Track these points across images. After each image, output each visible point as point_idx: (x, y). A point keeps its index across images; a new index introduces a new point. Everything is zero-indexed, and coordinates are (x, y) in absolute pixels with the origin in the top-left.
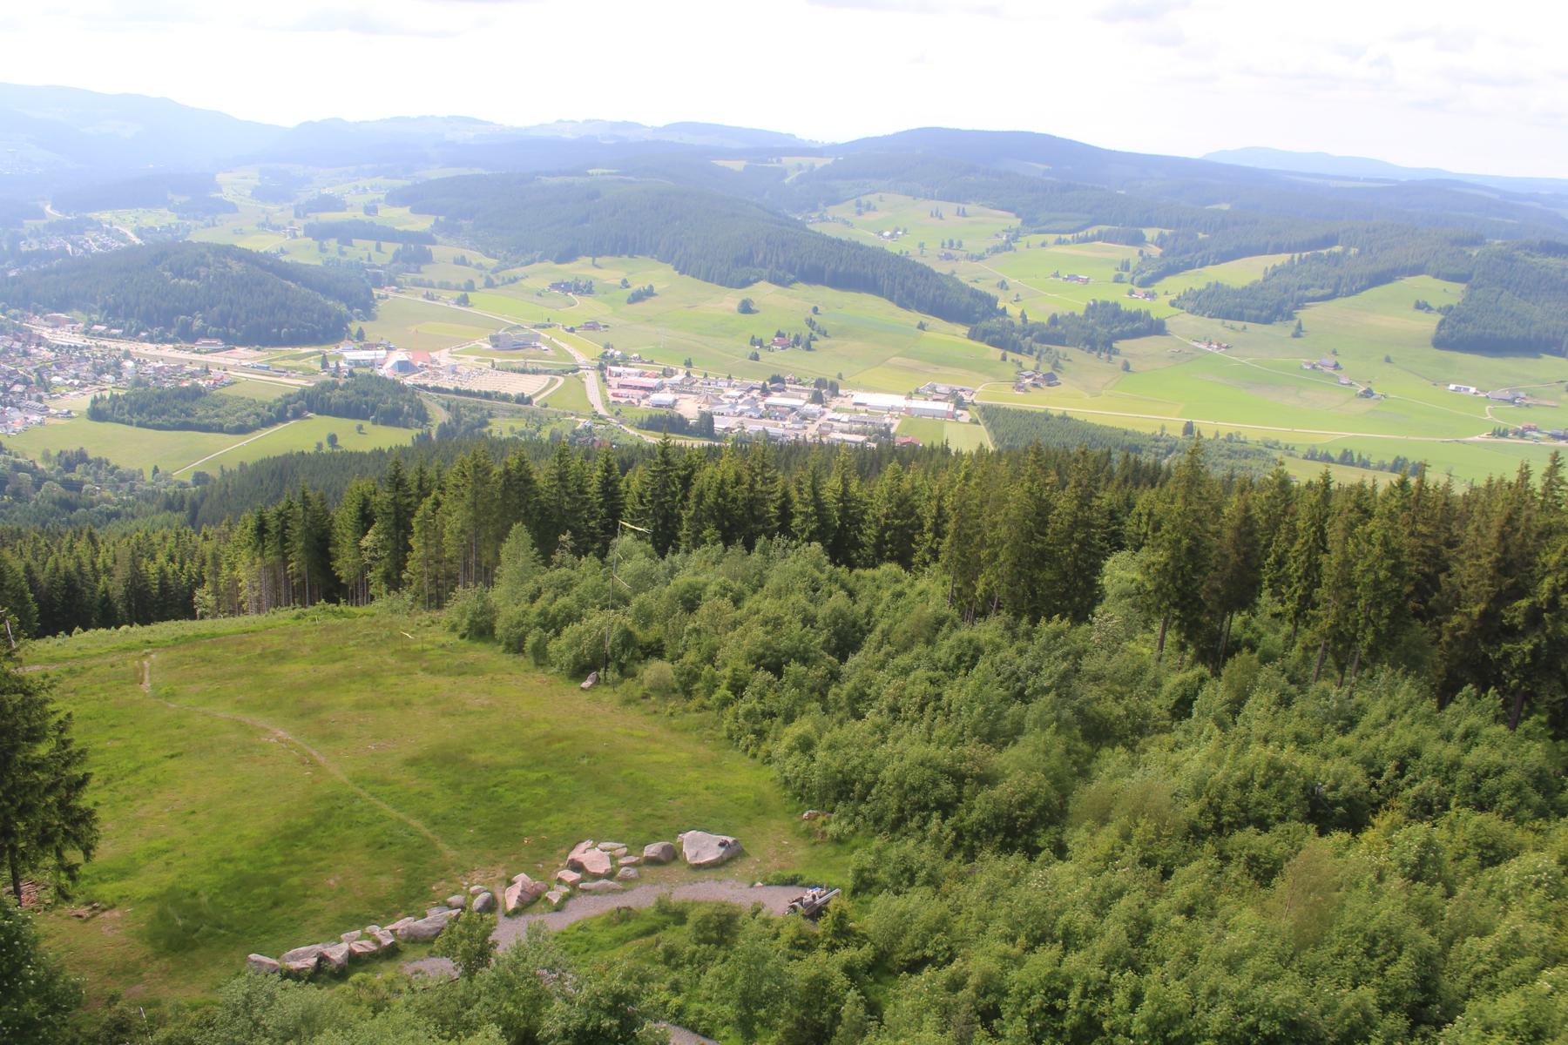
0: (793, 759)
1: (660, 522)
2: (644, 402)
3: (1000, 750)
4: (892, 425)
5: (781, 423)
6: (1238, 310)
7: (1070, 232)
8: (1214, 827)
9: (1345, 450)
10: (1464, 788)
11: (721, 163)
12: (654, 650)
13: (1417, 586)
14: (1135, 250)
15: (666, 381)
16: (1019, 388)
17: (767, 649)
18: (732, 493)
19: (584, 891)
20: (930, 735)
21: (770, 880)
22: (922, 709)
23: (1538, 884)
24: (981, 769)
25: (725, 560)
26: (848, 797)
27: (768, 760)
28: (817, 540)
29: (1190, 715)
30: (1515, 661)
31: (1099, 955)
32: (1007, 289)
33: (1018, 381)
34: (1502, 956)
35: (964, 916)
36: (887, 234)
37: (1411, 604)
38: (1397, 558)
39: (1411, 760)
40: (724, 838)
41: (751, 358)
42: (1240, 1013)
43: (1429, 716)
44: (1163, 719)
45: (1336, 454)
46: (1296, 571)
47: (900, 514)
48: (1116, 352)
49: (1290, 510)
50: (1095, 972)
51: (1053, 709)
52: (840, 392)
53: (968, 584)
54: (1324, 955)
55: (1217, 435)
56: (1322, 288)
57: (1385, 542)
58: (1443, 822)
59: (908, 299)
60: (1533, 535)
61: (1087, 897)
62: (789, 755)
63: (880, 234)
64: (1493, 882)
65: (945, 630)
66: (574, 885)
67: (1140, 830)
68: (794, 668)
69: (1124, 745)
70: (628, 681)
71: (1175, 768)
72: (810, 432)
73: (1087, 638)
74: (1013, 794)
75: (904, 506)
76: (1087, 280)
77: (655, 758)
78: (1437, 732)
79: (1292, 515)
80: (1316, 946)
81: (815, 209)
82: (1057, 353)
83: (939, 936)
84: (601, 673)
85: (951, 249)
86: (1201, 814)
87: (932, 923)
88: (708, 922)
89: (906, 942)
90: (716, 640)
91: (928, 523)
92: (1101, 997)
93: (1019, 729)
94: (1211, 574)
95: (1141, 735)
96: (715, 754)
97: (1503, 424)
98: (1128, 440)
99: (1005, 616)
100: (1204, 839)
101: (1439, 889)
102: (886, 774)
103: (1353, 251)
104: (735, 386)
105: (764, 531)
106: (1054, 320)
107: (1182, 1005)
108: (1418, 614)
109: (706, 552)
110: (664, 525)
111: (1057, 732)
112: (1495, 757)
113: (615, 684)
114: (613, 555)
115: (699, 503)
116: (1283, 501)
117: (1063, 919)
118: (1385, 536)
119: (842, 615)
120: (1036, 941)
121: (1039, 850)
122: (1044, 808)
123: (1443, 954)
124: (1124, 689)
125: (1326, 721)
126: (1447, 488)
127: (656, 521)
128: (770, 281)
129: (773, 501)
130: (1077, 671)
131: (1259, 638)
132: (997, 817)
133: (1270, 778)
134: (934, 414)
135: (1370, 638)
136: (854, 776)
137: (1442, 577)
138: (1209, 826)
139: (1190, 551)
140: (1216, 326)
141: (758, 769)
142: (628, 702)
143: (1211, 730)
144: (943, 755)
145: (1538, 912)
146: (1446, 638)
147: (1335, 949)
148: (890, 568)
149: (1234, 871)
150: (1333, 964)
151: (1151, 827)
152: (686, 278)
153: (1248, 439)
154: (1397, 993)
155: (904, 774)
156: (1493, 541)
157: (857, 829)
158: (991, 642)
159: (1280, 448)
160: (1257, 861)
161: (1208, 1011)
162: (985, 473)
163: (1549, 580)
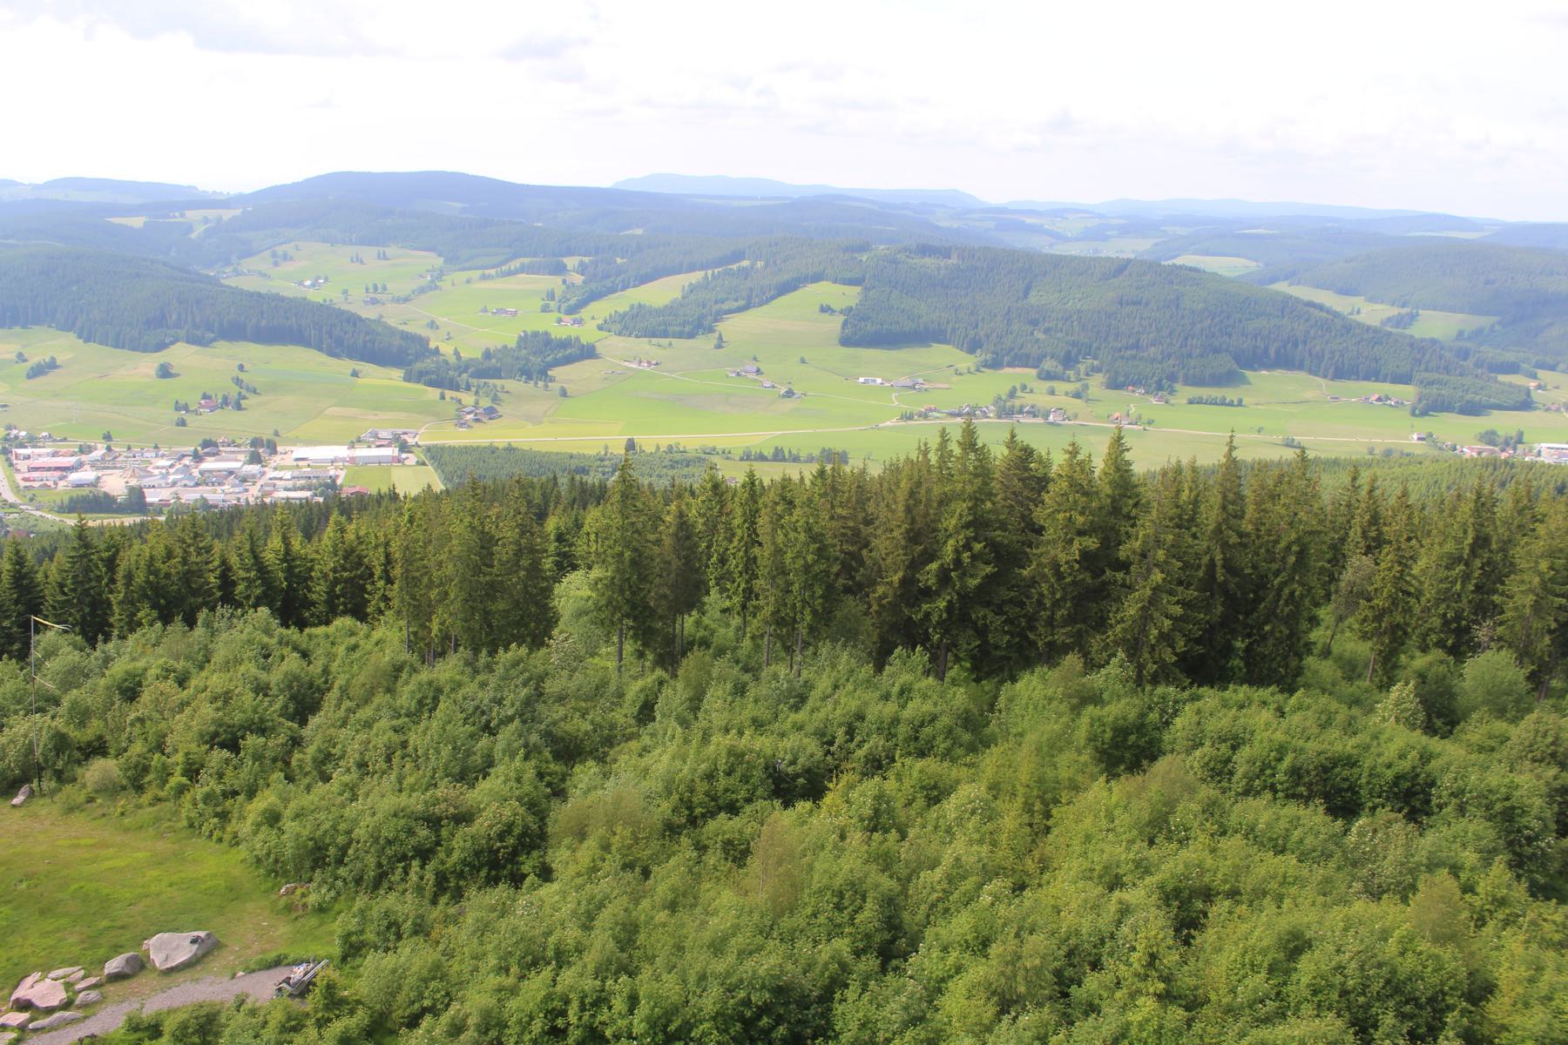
0: (261, 836)
1: (87, 610)
2: (62, 484)
3: (472, 786)
4: (337, 476)
5: (219, 489)
7: (493, 267)
8: (688, 821)
11: (117, 220)
12: (97, 749)
13: (843, 563)
14: (558, 280)
15: (84, 458)
16: (462, 425)
17: (221, 726)
18: (164, 568)
19: (35, 1030)
20: (400, 783)
21: (252, 966)
22: (389, 759)
23: (973, 812)
24: (456, 808)
25: (164, 640)
26: (325, 864)
27: (236, 841)
28: (266, 605)
29: (654, 719)
30: (935, 618)
31: (591, 967)
32: (438, 328)
33: (459, 418)
34: (950, 882)
35: (458, 958)
36: (308, 283)
37: (841, 581)
38: (821, 541)
40: (196, 934)
41: (178, 425)
42: (730, 990)
45: (768, 452)
46: (737, 566)
47: (348, 566)
48: (552, 380)
49: (725, 511)
50: (590, 984)
51: (520, 736)
52: (279, 449)
53: (423, 626)
54: (799, 920)
55: (658, 448)
56: (736, 300)
57: (809, 530)
58: (891, 774)
59: (337, 348)
60: (935, 505)
61: (574, 913)
62: (256, 833)
63: (301, 283)
64: (938, 818)
65: (404, 675)
66: (22, 1028)
67: (617, 837)
68: (252, 741)
69: (594, 758)
70: (68, 787)
71: (646, 772)
72: (252, 494)
73: (546, 661)
74: (491, 826)
75: (351, 557)
76: (515, 314)
77: (107, 864)
79: (727, 514)
80: (791, 912)
81: (228, 263)
82: (495, 386)
83: (433, 984)
84: (35, 784)
85: (375, 295)
86: (673, 811)
87: (425, 973)
88: (186, 1028)
89: (401, 998)
90: (163, 725)
91: (378, 571)
92: (599, 1007)
93: (489, 763)
94: (657, 581)
95: (611, 746)
96: (176, 847)
97: (908, 408)
98: (574, 463)
99: (464, 653)
100: (680, 834)
101: (893, 835)
102: (360, 833)
103: (760, 264)
104: (163, 456)
105: (205, 604)
106: (488, 355)
107: (676, 997)
108: (848, 590)
109: (144, 635)
110: (93, 614)
111: (526, 758)
112: (928, 707)
113: (53, 793)
114: (36, 654)
115: (128, 585)
116: (717, 503)
117: (552, 939)
119: (296, 678)
120: (534, 963)
121: (524, 876)
122: (524, 834)
123: (904, 892)
124: (589, 704)
125: (779, 702)
126: (863, 472)
127: (82, 609)
128: (188, 342)
129: (212, 571)
130: (542, 694)
131: (712, 635)
132: (477, 854)
134: (379, 461)
135: (808, 618)
136: (327, 841)
137: (864, 552)
138: (684, 821)
139: (634, 562)
140: (644, 346)
141: (227, 853)
142: (71, 810)
143: (674, 729)
144: (415, 802)
145: (976, 836)
146: (875, 607)
147: (809, 911)
148: (343, 622)
149: (711, 859)
150: (809, 924)
151: (627, 832)
152: (94, 346)
154: (868, 936)
155: (378, 829)
156: (900, 514)
157: (338, 894)
158: (452, 680)
161: (700, 996)
162: (424, 514)
163: (951, 542)
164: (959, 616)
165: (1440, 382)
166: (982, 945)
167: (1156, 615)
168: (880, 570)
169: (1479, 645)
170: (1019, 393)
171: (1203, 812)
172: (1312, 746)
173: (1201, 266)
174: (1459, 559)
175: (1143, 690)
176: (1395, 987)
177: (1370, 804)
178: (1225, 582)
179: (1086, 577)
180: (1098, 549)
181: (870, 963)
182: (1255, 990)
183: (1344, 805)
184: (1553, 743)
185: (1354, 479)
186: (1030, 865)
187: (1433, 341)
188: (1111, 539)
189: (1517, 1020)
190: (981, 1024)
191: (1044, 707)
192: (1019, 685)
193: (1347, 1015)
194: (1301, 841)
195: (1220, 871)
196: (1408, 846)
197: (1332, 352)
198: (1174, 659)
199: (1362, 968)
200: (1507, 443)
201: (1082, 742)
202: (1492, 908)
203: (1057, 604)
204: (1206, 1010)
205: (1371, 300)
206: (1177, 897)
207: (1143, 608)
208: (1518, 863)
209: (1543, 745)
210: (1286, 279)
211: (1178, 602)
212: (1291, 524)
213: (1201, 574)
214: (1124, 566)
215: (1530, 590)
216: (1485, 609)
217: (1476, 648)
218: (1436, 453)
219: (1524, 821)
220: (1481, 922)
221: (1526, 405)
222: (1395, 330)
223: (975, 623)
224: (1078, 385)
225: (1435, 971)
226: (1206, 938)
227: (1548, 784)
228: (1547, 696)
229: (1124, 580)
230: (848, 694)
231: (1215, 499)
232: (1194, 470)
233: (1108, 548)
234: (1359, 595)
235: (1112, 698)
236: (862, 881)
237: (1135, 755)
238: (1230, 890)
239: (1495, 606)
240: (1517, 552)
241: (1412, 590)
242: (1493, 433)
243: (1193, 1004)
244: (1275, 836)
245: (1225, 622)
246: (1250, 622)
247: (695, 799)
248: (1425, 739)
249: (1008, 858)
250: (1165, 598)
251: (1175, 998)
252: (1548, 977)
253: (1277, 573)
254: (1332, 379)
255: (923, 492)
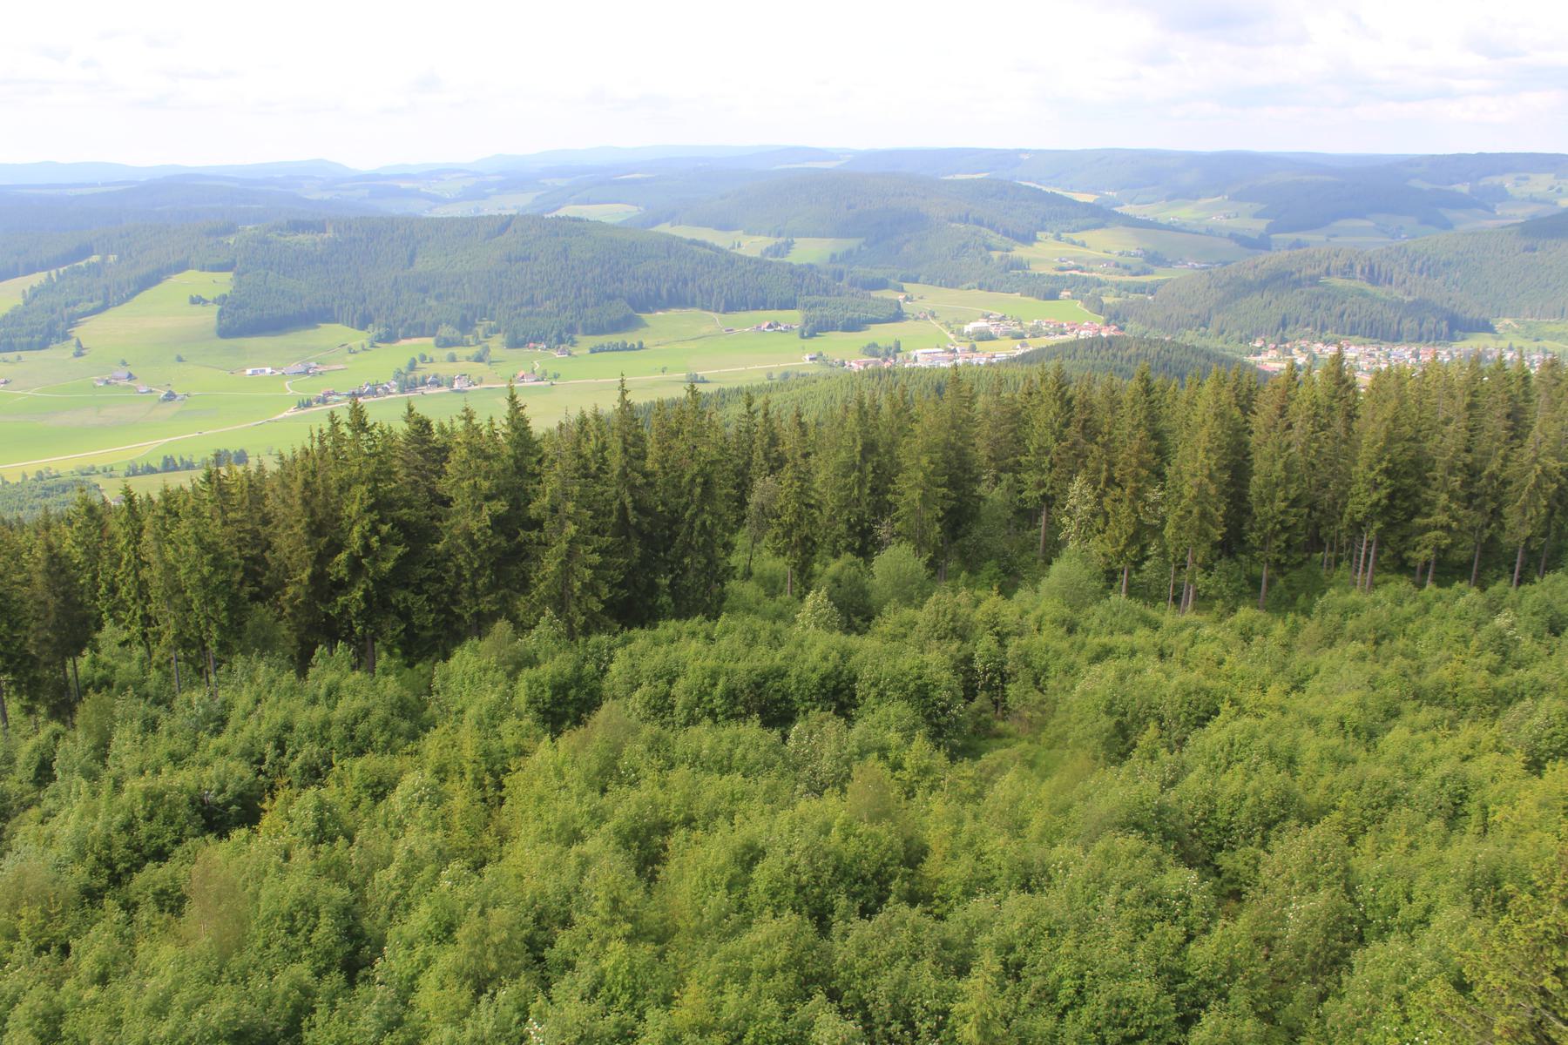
6: (6, 340)
8: (110, 881)
9: (165, 458)
10: (340, 741)
13: (245, 569)
23: (421, 800)
30: (353, 610)
34: (407, 877)
37: (247, 589)
38: (216, 551)
39: (287, 735)
43: (292, 688)
44: (28, 792)
45: (157, 463)
49: (106, 534)
54: (250, 956)
55: (25, 476)
56: (91, 301)
57: (199, 540)
60: (335, 492)
64: (386, 815)
67: (24, 921)
78: (304, 700)
86: (91, 874)
94: (34, 625)
97: (305, 396)
100: (102, 897)
103: (112, 258)
108: (255, 597)
112: (359, 703)
118: (196, 534)
123: (361, 899)
125: (197, 730)
131: (113, 672)
133: (152, 808)
137: (267, 554)
138: (105, 882)
145: (428, 824)
147: (260, 943)
149: (143, 916)
151: (36, 911)
153: (62, 471)
154: (328, 953)
159: (98, 473)
160: (167, 894)
163: (357, 528)
164: (378, 604)
165: (821, 304)
166: (446, 931)
167: (577, 567)
168: (286, 570)
169: (881, 543)
170: (419, 365)
171: (649, 750)
172: (742, 666)
173: (585, 216)
174: (854, 466)
175: (577, 642)
176: (843, 872)
177: (803, 708)
178: (638, 523)
179: (502, 541)
180: (508, 511)
181: (336, 979)
182: (718, 907)
183: (778, 714)
184: (952, 620)
185: (749, 405)
186: (488, 839)
187: (811, 266)
188: (520, 500)
189: (948, 871)
190: (459, 1012)
191: (480, 679)
192: (452, 662)
193: (805, 908)
194: (744, 757)
195: (672, 803)
196: (839, 740)
197: (721, 287)
198: (601, 607)
199: (811, 862)
200: (888, 354)
201: (523, 706)
202: (919, 778)
203: (476, 574)
204: (678, 939)
205: (749, 233)
206: (636, 838)
207: (562, 562)
208: (937, 734)
209: (945, 623)
210: (667, 221)
211: (594, 551)
212: (692, 457)
213: (613, 519)
214: (537, 524)
215: (917, 485)
216: (882, 509)
217: (880, 546)
218: (827, 370)
219: (936, 694)
220: (910, 794)
221: (898, 316)
222: (774, 260)
223: (396, 607)
224: (478, 349)
225: (876, 847)
226: (669, 871)
227: (952, 657)
228: (946, 579)
229: (539, 537)
230: (273, 706)
231: (616, 445)
232: (597, 418)
233: (518, 508)
234: (767, 514)
235: (546, 656)
236: (312, 897)
237: (577, 709)
238: (685, 818)
239: (891, 505)
240: (901, 452)
241: (813, 502)
242: (875, 345)
243: (663, 937)
244: (719, 758)
245: (645, 562)
246: (669, 558)
247: (115, 856)
248: (844, 638)
249: (464, 838)
250: (582, 548)
251: (645, 935)
252: (968, 826)
253: (686, 507)
254: (724, 312)
255: (319, 481)
